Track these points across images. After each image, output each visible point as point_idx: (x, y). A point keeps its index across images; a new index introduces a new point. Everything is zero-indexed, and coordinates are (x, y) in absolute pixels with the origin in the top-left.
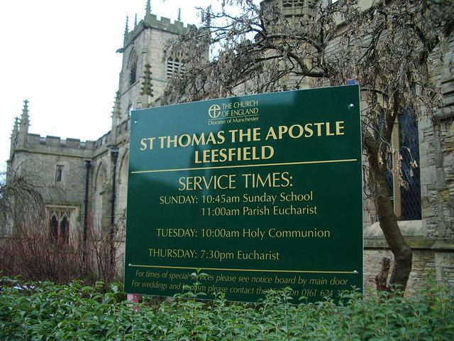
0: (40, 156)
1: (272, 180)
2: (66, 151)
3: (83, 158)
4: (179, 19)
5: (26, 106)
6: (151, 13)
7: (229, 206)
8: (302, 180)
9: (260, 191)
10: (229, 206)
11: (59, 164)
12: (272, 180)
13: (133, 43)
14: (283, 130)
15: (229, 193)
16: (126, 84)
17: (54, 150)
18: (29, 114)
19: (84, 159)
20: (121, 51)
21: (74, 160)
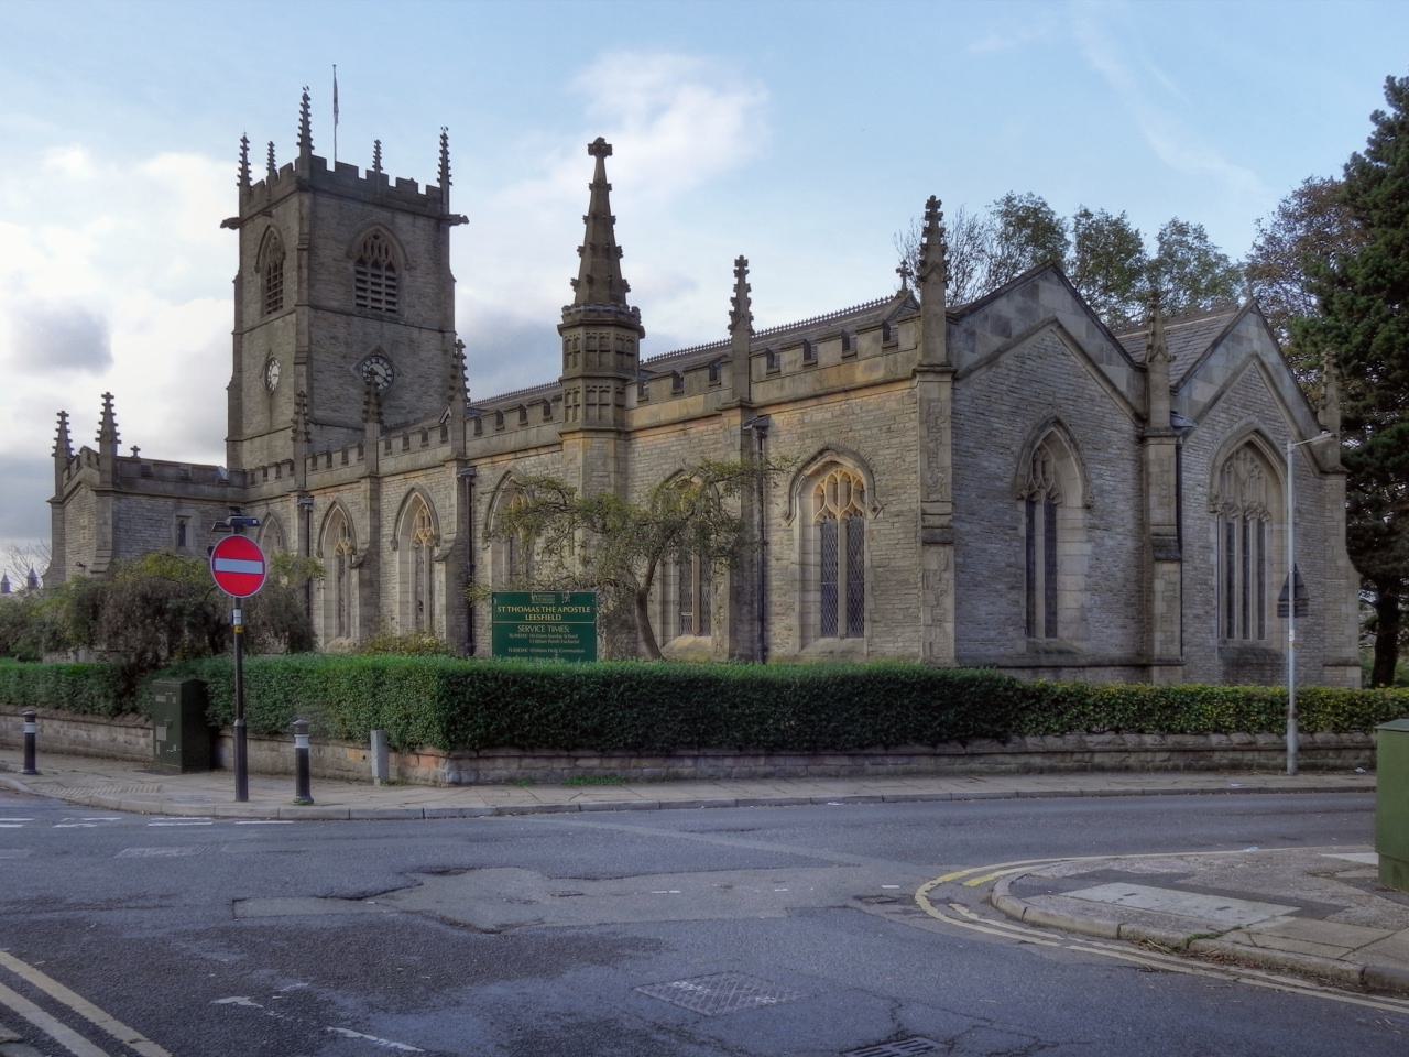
0: (143, 500)
1: (561, 629)
2: (191, 489)
3: (225, 502)
4: (377, 165)
5: (108, 406)
6: (314, 153)
7: (543, 639)
8: (573, 629)
9: (555, 633)
10: (543, 639)
11: (179, 514)
12: (561, 629)
13: (270, 215)
14: (565, 608)
15: (543, 634)
16: (254, 309)
17: (170, 487)
18: (116, 419)
19: (228, 505)
20: (229, 223)
21: (209, 507)
